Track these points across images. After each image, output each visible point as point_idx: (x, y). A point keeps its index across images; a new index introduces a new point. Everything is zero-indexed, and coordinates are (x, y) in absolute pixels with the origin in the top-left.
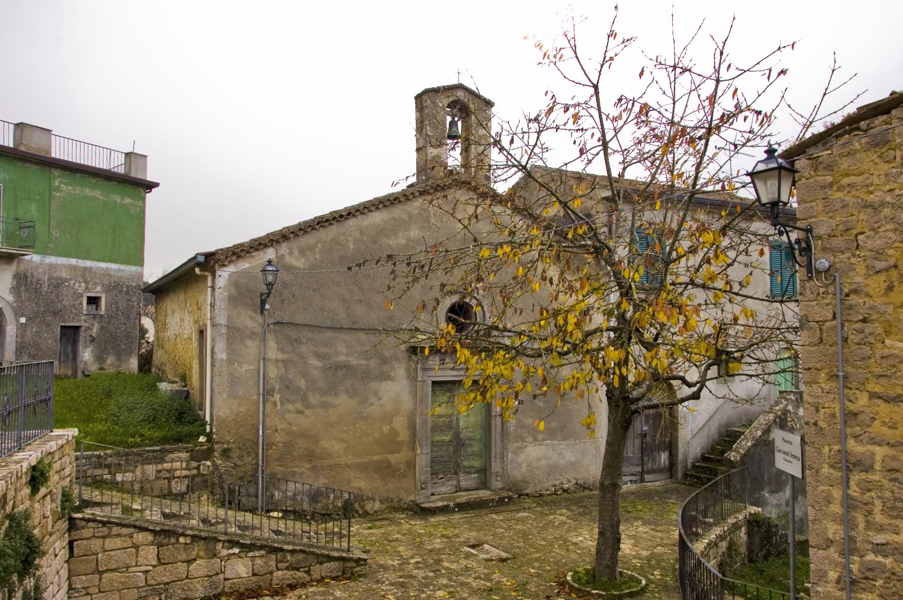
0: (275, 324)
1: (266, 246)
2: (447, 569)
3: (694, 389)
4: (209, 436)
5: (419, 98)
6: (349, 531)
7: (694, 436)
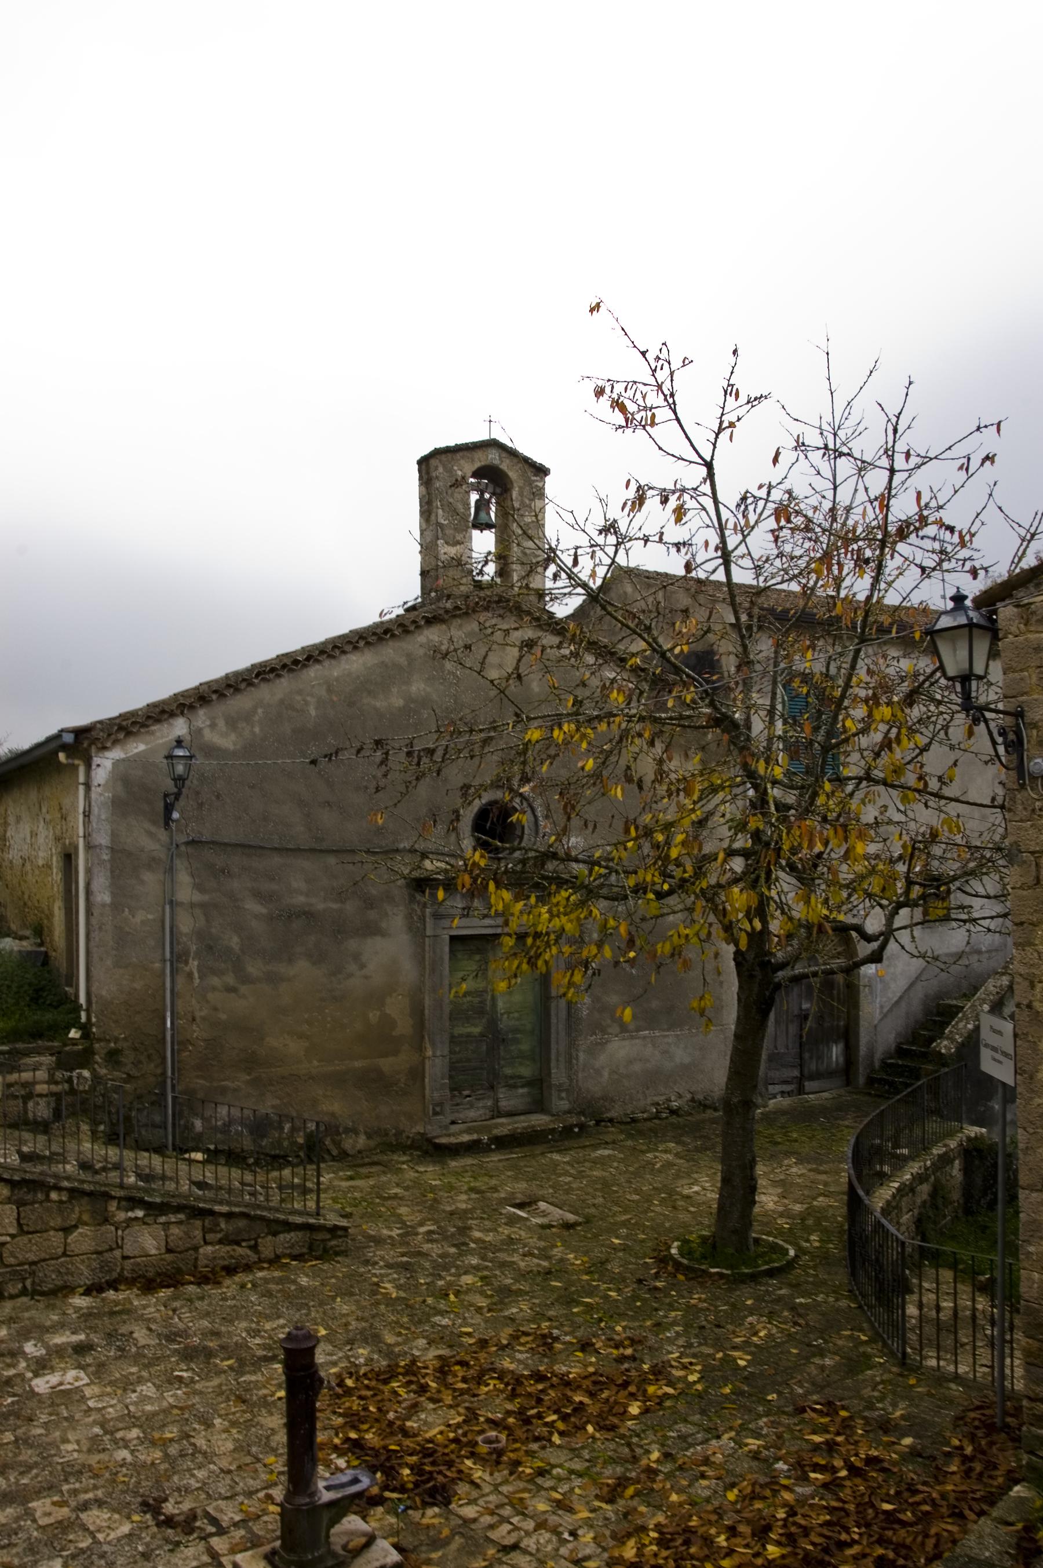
0: (187, 843)
1: (172, 715)
2: (477, 1241)
3: (875, 945)
4: (85, 1028)
5: (420, 462)
6: (318, 1183)
7: (885, 1016)
